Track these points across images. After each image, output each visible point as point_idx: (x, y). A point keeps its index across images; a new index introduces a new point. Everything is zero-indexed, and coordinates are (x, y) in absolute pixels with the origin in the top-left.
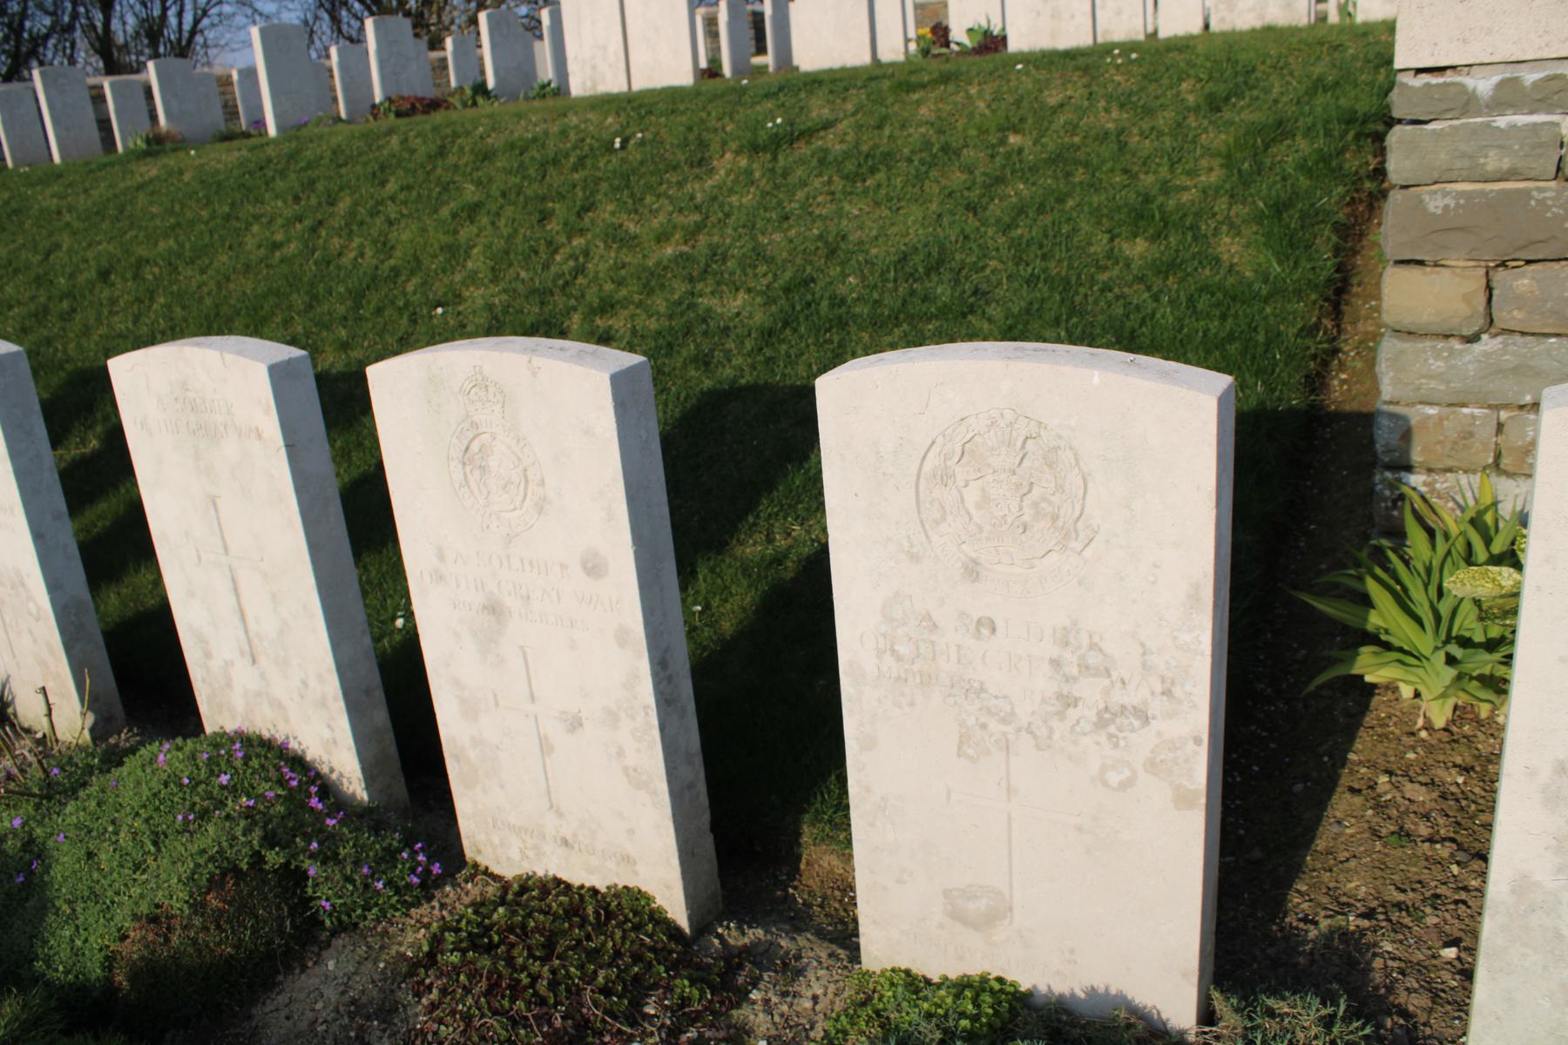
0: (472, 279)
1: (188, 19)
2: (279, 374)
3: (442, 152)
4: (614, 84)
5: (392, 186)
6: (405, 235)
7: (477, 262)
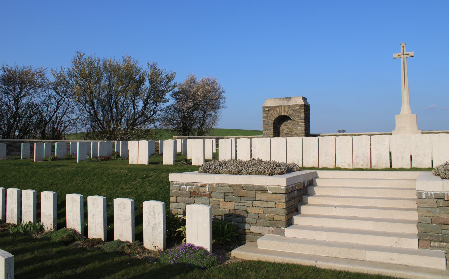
0: (103, 192)
1: (62, 128)
2: (81, 197)
3: (103, 173)
4: (135, 163)
5: (95, 177)
6: (96, 185)
7: (104, 189)
